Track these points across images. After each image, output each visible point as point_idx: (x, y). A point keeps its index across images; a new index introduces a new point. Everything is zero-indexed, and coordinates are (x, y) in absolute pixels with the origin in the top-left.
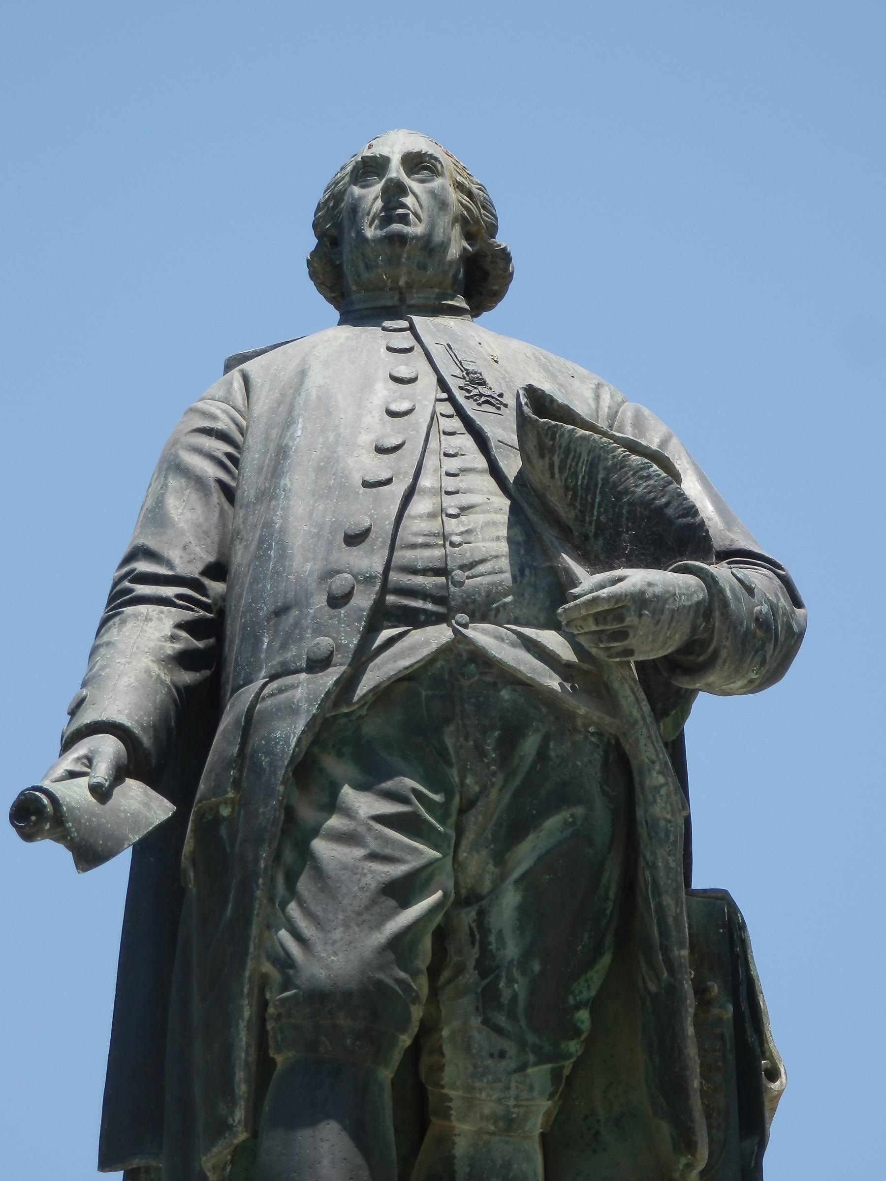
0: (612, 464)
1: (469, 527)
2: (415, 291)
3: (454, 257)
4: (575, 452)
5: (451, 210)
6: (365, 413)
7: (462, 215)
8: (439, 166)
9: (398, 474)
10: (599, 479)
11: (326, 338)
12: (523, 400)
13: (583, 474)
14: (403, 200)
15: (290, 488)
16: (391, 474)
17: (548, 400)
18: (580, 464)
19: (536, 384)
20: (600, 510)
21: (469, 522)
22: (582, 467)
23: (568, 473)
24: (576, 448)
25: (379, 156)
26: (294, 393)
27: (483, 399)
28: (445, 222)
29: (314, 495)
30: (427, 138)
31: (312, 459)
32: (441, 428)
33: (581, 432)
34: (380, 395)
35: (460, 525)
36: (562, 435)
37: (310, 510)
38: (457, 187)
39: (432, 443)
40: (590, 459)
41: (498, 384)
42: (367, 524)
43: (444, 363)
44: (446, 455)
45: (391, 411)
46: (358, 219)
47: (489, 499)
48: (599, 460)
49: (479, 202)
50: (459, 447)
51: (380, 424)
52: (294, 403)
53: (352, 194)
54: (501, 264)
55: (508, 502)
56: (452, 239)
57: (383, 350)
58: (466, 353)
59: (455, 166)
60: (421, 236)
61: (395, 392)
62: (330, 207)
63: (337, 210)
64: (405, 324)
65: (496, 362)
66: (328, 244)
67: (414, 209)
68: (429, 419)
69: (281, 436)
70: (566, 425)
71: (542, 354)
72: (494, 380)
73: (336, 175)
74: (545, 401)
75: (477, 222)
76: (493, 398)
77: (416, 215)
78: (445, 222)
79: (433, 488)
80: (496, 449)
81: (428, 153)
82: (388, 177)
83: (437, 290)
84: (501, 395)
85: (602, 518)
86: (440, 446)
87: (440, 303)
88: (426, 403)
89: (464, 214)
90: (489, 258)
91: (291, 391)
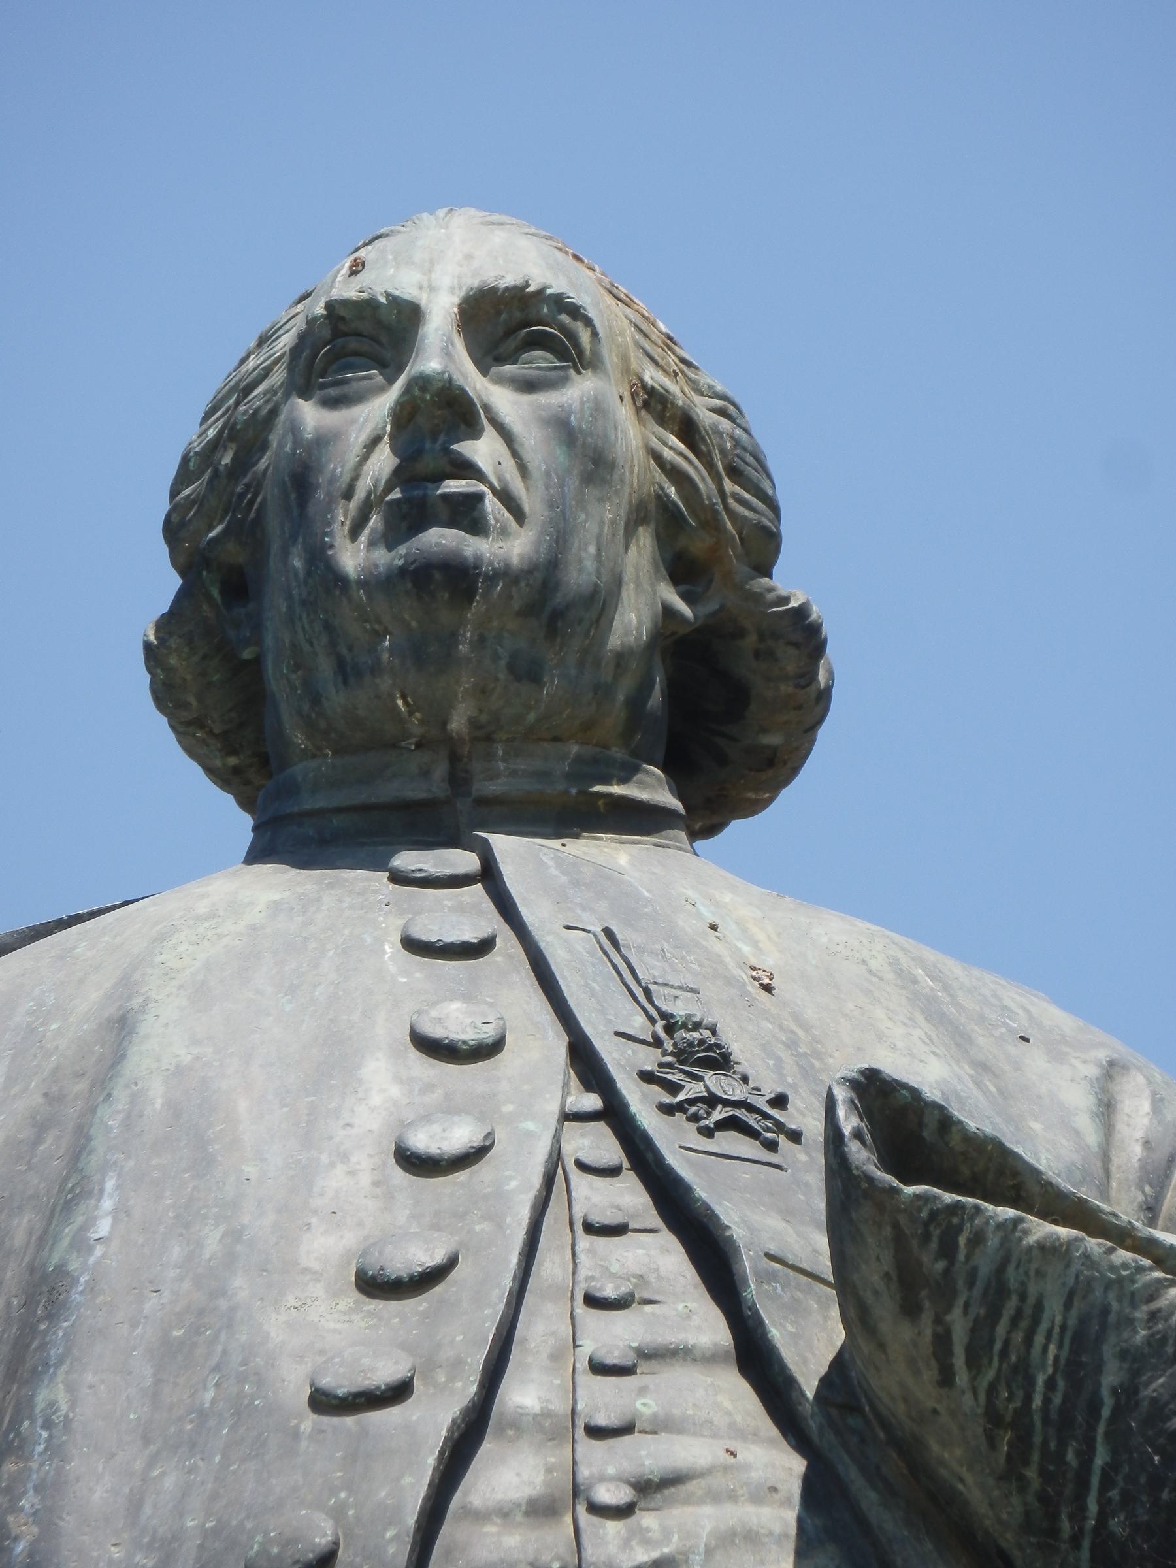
0: (1149, 1341)
1: (666, 1550)
2: (500, 753)
3: (632, 639)
4: (1023, 1297)
5: (622, 481)
6: (324, 1158)
7: (662, 500)
8: (585, 337)
9: (430, 1366)
10: (1105, 1393)
11: (202, 908)
12: (848, 1122)
13: (1050, 1370)
14: (466, 448)
15: (66, 1416)
16: (409, 1366)
17: (931, 1120)
18: (1039, 1339)
19: (893, 1066)
20: (1110, 1494)
21: (666, 1534)
22: (1045, 1349)
23: (999, 1370)
24: (1023, 1284)
25: (383, 300)
26: (91, 1092)
27: (719, 1114)
28: (602, 523)
29: (146, 1440)
30: (551, 238)
31: (146, 1317)
32: (579, 1211)
33: (1041, 1229)
34: (376, 1099)
35: (633, 1543)
36: (978, 1239)
37: (131, 1490)
38: (646, 405)
39: (548, 1264)
40: (1072, 1322)
41: (771, 1062)
42: (322, 1540)
43: (593, 994)
44: (594, 1301)
45: (412, 1153)
46: (311, 509)
47: (733, 1454)
48: (1104, 1326)
49: (717, 457)
50: (634, 1276)
51: (376, 1197)
52: (91, 1126)
53: (294, 428)
54: (790, 659)
55: (797, 1465)
56: (626, 579)
57: (392, 948)
58: (665, 958)
59: (638, 336)
60: (522, 571)
61: (428, 1088)
62: (221, 468)
63: (246, 480)
64: (465, 861)
65: (768, 988)
66: (215, 593)
67: (500, 480)
68: (537, 1181)
69: (45, 1238)
70: (990, 1207)
71: (919, 961)
72: (758, 1052)
73: (243, 361)
74: (921, 1125)
75: (711, 522)
76: (751, 1108)
77: (506, 498)
78: (602, 523)
79: (546, 1414)
80: (760, 1283)
81: (549, 291)
82: (413, 372)
83: (574, 749)
84: (780, 1101)
85: (1117, 1525)
86: (574, 1273)
87: (584, 793)
88: (530, 1125)
89: (668, 496)
90: (751, 640)
91: (82, 1086)
